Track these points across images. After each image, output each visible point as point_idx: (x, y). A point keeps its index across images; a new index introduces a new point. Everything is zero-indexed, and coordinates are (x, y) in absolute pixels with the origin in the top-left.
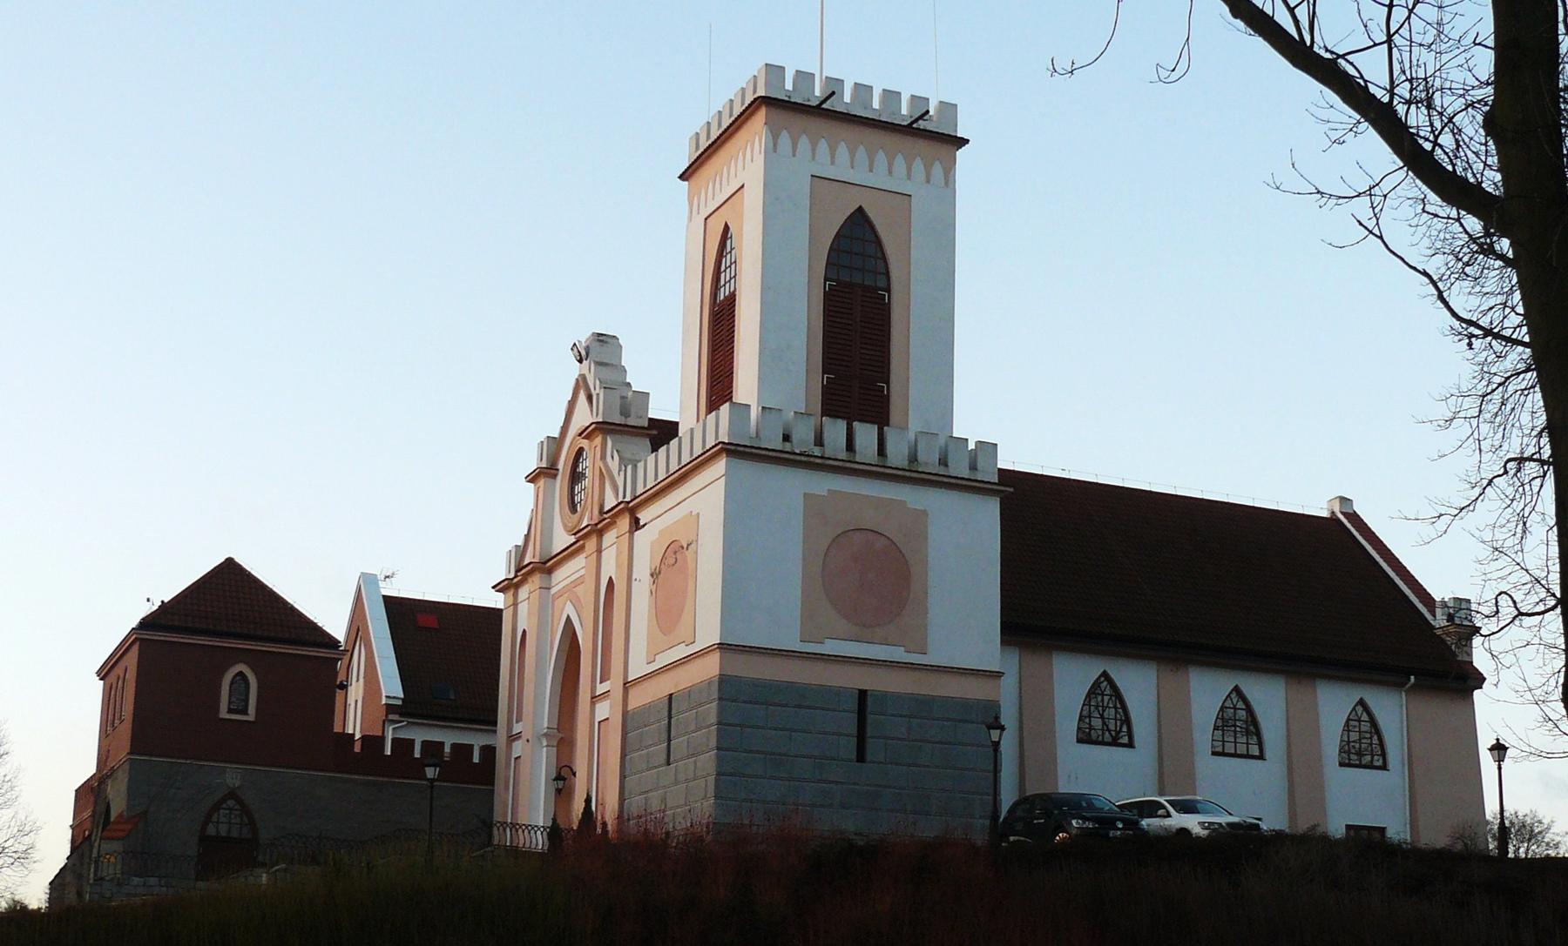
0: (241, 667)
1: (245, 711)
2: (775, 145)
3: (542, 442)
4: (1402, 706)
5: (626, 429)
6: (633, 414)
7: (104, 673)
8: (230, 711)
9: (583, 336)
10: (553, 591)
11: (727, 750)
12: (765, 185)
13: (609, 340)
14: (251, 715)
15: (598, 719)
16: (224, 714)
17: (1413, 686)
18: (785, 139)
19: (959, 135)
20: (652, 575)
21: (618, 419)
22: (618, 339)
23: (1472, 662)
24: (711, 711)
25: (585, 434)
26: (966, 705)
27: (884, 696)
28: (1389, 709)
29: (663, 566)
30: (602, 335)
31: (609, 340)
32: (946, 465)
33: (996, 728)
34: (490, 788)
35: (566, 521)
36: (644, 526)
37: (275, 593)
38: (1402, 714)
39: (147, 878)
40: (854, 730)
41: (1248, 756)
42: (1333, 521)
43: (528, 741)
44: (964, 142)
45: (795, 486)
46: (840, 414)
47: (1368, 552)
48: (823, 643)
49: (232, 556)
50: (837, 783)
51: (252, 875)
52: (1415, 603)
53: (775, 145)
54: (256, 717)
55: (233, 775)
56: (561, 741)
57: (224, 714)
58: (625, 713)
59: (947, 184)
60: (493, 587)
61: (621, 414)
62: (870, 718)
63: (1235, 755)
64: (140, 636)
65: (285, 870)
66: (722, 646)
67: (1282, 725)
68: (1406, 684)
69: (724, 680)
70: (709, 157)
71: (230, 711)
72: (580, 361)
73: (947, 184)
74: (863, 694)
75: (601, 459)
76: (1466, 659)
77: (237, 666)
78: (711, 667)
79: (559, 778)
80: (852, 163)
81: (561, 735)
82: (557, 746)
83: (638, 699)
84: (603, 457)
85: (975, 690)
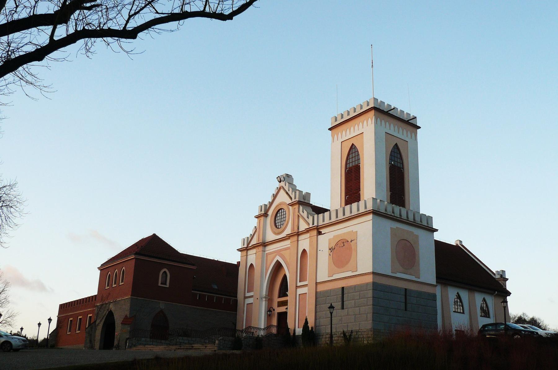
0: (165, 270)
1: (165, 284)
2: (377, 121)
3: (261, 206)
4: (492, 300)
5: (304, 203)
6: (306, 200)
7: (105, 269)
8: (161, 284)
9: (282, 173)
10: (266, 252)
11: (375, 305)
12: (375, 133)
13: (290, 176)
14: (168, 286)
15: (298, 294)
16: (160, 285)
17: (496, 295)
18: (379, 120)
19: (418, 125)
20: (330, 249)
21: (302, 200)
22: (292, 176)
23: (506, 289)
24: (370, 293)
25: (290, 204)
26: (429, 294)
27: (411, 290)
28: (490, 300)
29: (336, 247)
30: (288, 175)
31: (290, 176)
32: (422, 222)
33: (505, 302)
34: (236, 313)
35: (274, 231)
36: (324, 234)
37: (170, 246)
38: (493, 302)
39: (146, 339)
40: (404, 301)
41: (460, 313)
42: (457, 246)
43: (257, 299)
44: (419, 128)
45: (389, 225)
46: (349, 204)
47: (470, 256)
48: (396, 274)
49: (155, 233)
50: (401, 317)
51: (178, 339)
52: (488, 271)
53: (377, 121)
54: (169, 286)
55: (162, 305)
56: (269, 299)
57: (160, 285)
58: (316, 292)
59: (416, 139)
60: (237, 250)
61: (303, 199)
62: (408, 297)
63: (458, 312)
64: (136, 257)
65: (222, 339)
66: (374, 273)
67: (468, 305)
68: (494, 294)
69: (374, 284)
70: (344, 123)
71: (161, 284)
72: (280, 182)
73: (416, 139)
74: (406, 289)
75: (298, 212)
76: (505, 288)
77: (163, 269)
78: (369, 279)
79: (269, 311)
80: (394, 130)
81: (269, 297)
82: (268, 301)
83: (321, 288)
84: (299, 212)
85: (430, 290)
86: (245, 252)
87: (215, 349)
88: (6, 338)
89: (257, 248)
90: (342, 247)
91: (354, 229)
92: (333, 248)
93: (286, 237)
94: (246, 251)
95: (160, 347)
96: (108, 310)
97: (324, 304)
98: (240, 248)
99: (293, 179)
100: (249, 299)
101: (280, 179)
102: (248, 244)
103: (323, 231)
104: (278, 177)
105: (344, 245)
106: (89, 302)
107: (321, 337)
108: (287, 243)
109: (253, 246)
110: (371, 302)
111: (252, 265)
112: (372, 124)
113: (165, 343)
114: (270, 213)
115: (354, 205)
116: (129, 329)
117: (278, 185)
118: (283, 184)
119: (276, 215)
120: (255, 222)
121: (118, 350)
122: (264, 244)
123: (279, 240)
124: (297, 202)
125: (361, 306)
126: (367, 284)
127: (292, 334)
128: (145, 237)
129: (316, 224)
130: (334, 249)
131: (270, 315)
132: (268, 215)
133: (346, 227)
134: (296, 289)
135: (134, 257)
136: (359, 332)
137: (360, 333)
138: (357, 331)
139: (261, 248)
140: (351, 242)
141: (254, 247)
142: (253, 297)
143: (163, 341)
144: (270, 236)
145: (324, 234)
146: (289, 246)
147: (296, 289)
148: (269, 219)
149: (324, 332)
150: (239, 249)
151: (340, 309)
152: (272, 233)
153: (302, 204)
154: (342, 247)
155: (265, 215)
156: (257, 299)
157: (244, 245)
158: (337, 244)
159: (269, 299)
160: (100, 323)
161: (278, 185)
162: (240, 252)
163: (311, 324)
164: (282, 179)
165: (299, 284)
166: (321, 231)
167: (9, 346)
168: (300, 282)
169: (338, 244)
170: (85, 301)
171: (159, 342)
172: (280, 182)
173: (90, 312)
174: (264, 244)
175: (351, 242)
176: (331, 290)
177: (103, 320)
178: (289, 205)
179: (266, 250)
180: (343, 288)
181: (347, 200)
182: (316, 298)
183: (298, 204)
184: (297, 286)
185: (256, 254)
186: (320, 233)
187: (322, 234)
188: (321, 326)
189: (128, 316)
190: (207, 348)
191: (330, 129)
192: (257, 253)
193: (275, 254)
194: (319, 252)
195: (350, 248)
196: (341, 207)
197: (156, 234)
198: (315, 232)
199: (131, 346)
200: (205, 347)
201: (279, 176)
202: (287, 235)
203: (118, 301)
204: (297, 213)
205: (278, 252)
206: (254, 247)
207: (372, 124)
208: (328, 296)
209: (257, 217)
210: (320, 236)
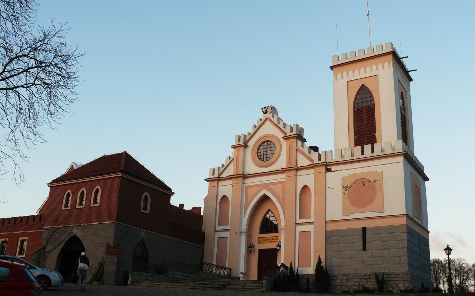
8: (143, 209)
36: (334, 171)
43: (236, 233)
51: (174, 274)
55: (143, 234)
58: (326, 231)
64: (123, 176)
70: (338, 66)
71: (143, 209)
83: (331, 227)
86: (215, 183)
87: (263, 290)
88: (41, 271)
89: (235, 180)
90: (361, 186)
91: (379, 169)
92: (349, 187)
93: (281, 170)
94: (217, 182)
95: (179, 285)
96: (69, 235)
97: (338, 244)
98: (209, 178)
99: (277, 112)
100: (220, 233)
101: (267, 110)
102: (219, 175)
103: (333, 168)
104: (264, 108)
105: (364, 185)
106: (9, 223)
107: (335, 278)
108: (281, 177)
109: (229, 177)
110: (405, 244)
111: (225, 197)
112: (390, 67)
113: (163, 279)
114: (251, 144)
115: (367, 148)
116: (116, 260)
117: (262, 116)
118: (268, 115)
119: (260, 145)
120: (230, 152)
121: (102, 284)
122: (245, 177)
123: (267, 173)
124: (297, 135)
125: (392, 249)
126: (399, 226)
127: (296, 274)
128: (106, 155)
129: (323, 160)
130: (350, 187)
131: (250, 251)
132: (248, 146)
133: (359, 168)
134: (296, 225)
135: (120, 175)
136: (391, 274)
137: (393, 276)
138: (388, 273)
139: (240, 180)
140: (375, 182)
141: (230, 178)
142: (229, 231)
143: (162, 277)
144: (251, 168)
145: (334, 171)
146: (285, 180)
147: (296, 225)
148: (249, 151)
149: (338, 273)
150: (207, 179)
151: (361, 250)
152: (255, 166)
153: (301, 139)
154: (361, 186)
155: (245, 146)
156: (236, 233)
157: (213, 174)
158: (354, 183)
159: (249, 236)
160: (54, 250)
161: (262, 116)
162: (208, 183)
163: (323, 264)
164: (269, 110)
165: (299, 221)
166: (330, 168)
167: (46, 283)
168: (300, 219)
169: (355, 183)
170: (30, 220)
171: (158, 278)
172: (265, 113)
173: (23, 235)
174: (245, 177)
175: (375, 182)
176: (346, 230)
177: (61, 247)
178: (284, 138)
179: (246, 183)
180: (364, 229)
181: (357, 140)
182: (326, 237)
183: (296, 138)
184: (296, 223)
185: (233, 185)
186: (328, 170)
187: (331, 171)
188: (333, 266)
189: (112, 244)
190: (245, 287)
191: (332, 68)
192: (234, 185)
193: (260, 187)
194: (327, 189)
195: (374, 189)
196: (349, 147)
197: (127, 152)
198: (323, 169)
199: (133, 282)
200: (242, 287)
201: (265, 107)
202: (282, 169)
203: (91, 225)
204: (295, 147)
205: (265, 186)
206: (230, 178)
207: (390, 67)
208: (343, 236)
209: (233, 147)
210: (328, 174)
